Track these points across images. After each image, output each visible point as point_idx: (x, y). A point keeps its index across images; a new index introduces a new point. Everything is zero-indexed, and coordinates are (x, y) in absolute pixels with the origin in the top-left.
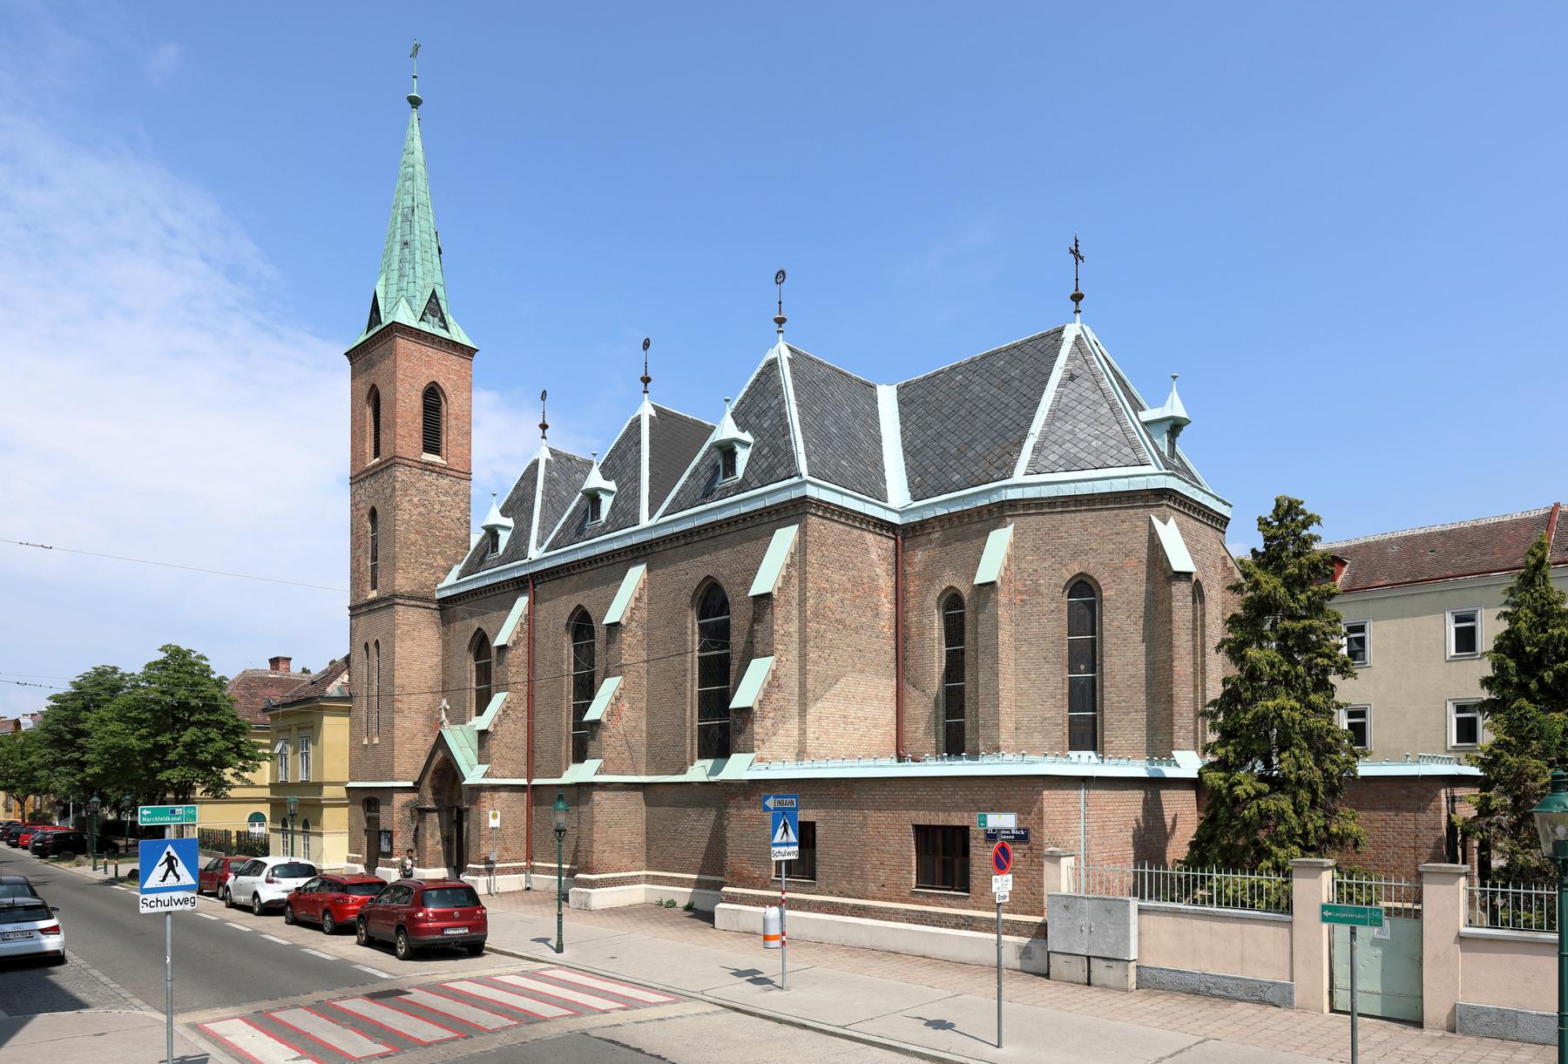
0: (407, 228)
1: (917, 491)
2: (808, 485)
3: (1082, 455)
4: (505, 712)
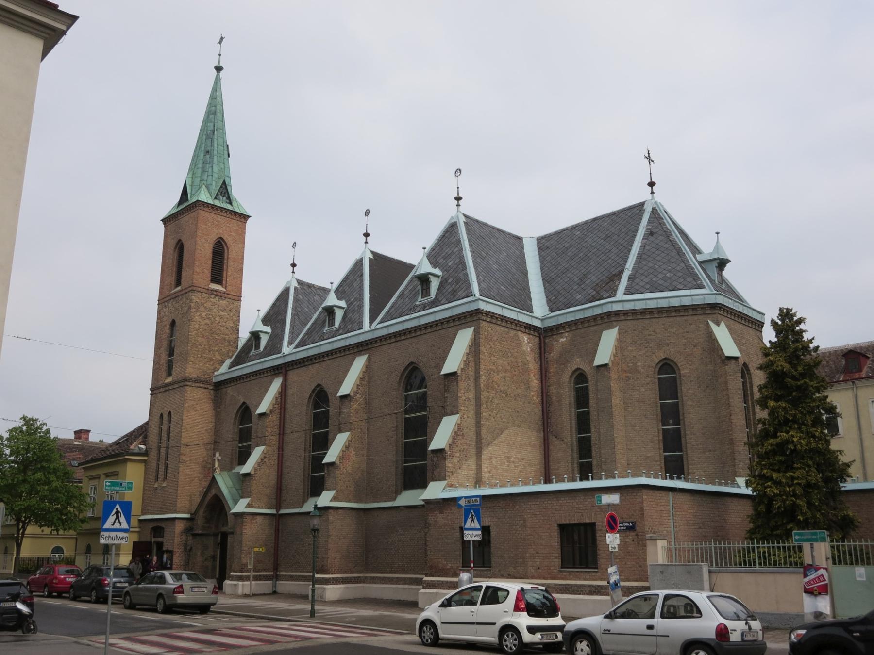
0: (209, 142)
1: (553, 304)
2: (480, 301)
3: (661, 282)
4: (262, 461)
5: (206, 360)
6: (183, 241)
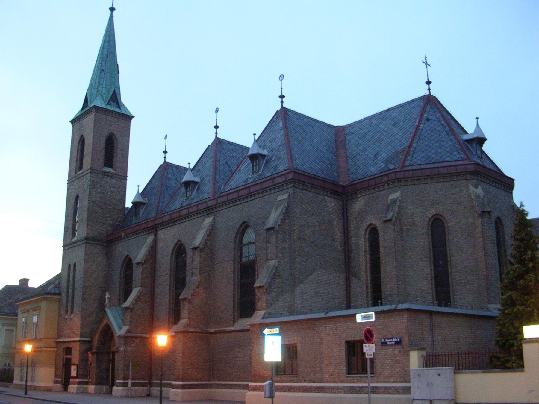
4: (138, 299)
5: (101, 224)
6: (85, 137)
